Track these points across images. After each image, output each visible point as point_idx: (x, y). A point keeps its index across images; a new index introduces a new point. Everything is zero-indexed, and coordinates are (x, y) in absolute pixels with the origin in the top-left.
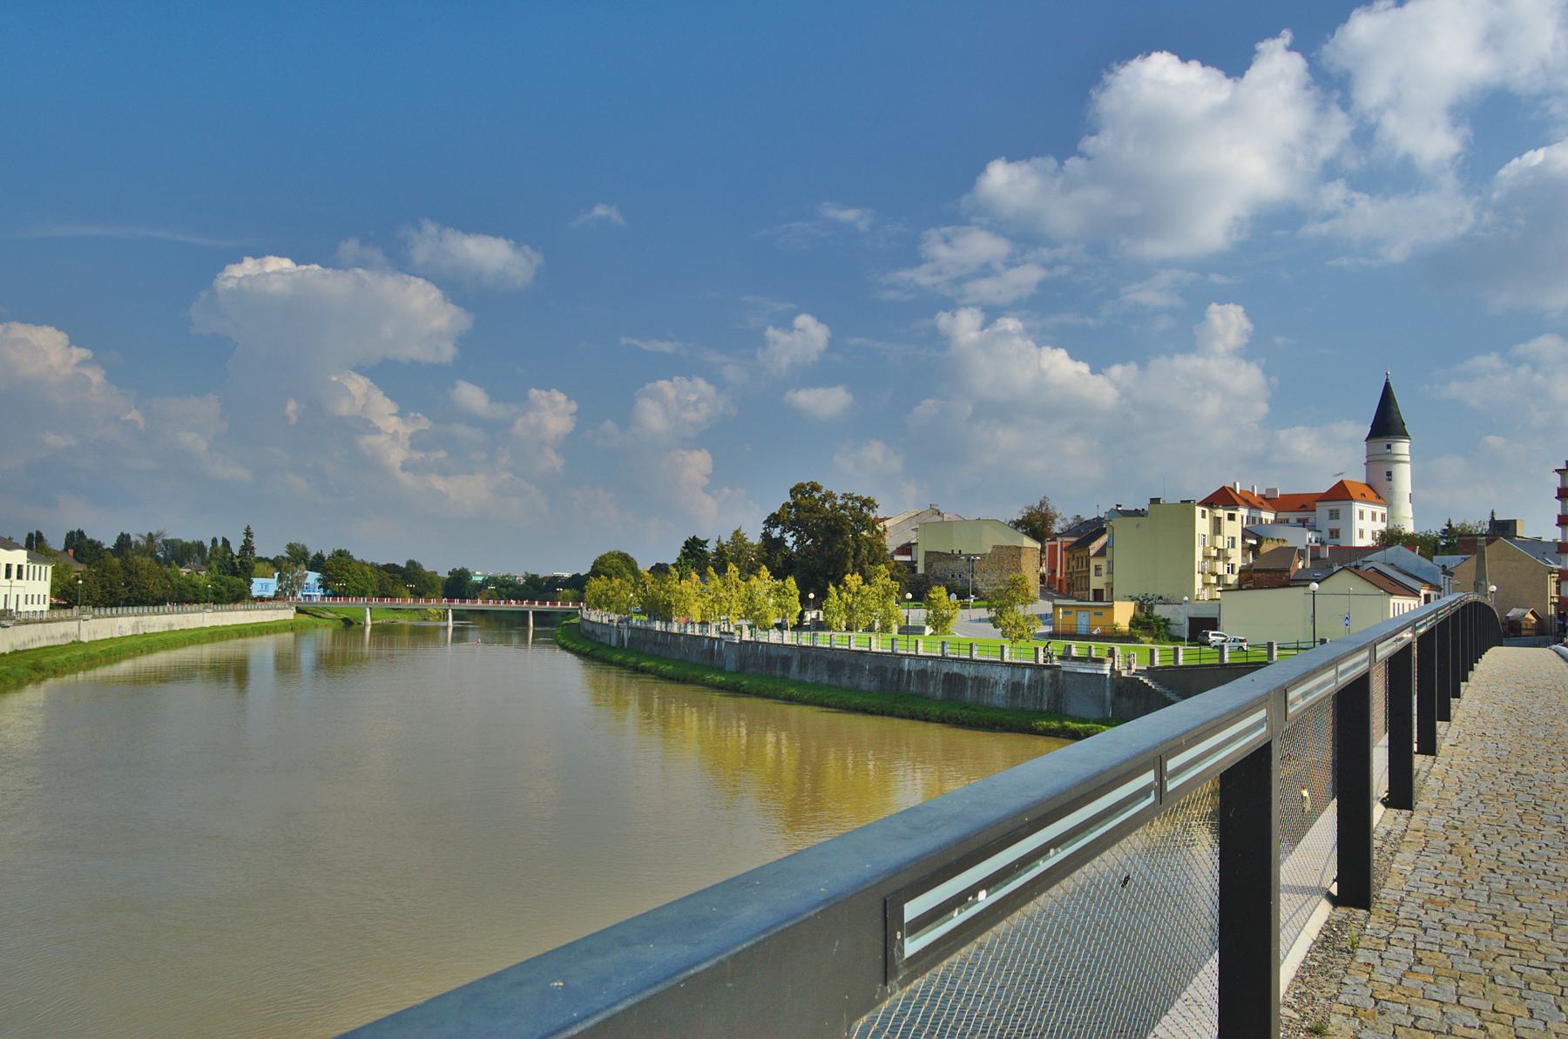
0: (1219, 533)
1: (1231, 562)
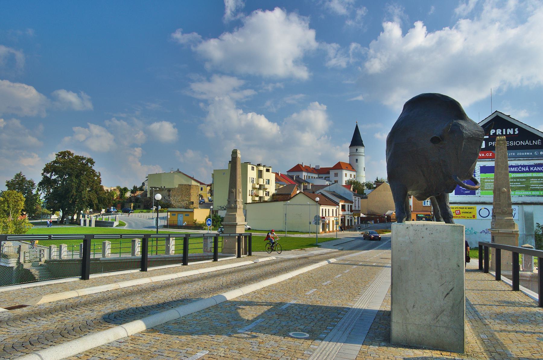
0: (261, 177)
1: (267, 191)
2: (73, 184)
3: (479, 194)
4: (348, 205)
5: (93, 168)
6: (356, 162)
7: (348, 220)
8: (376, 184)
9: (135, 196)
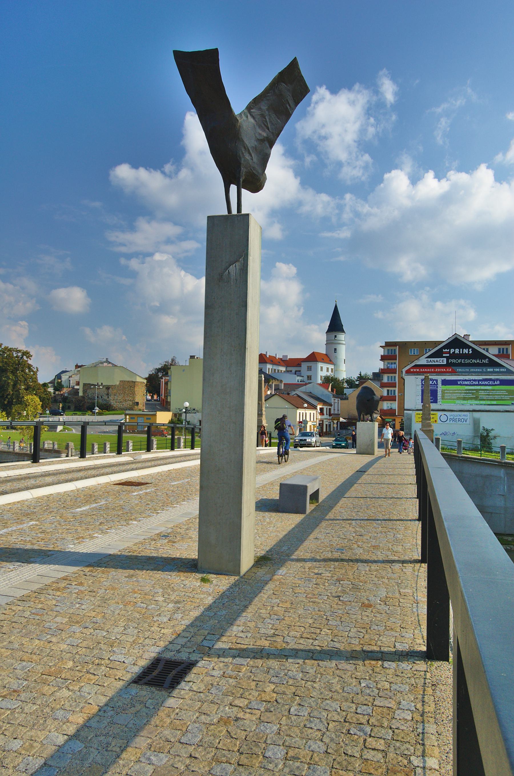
2: (9, 381)
3: (440, 403)
4: (327, 408)
5: (30, 362)
6: (335, 352)
7: (326, 425)
8: (359, 381)
9: (61, 395)
